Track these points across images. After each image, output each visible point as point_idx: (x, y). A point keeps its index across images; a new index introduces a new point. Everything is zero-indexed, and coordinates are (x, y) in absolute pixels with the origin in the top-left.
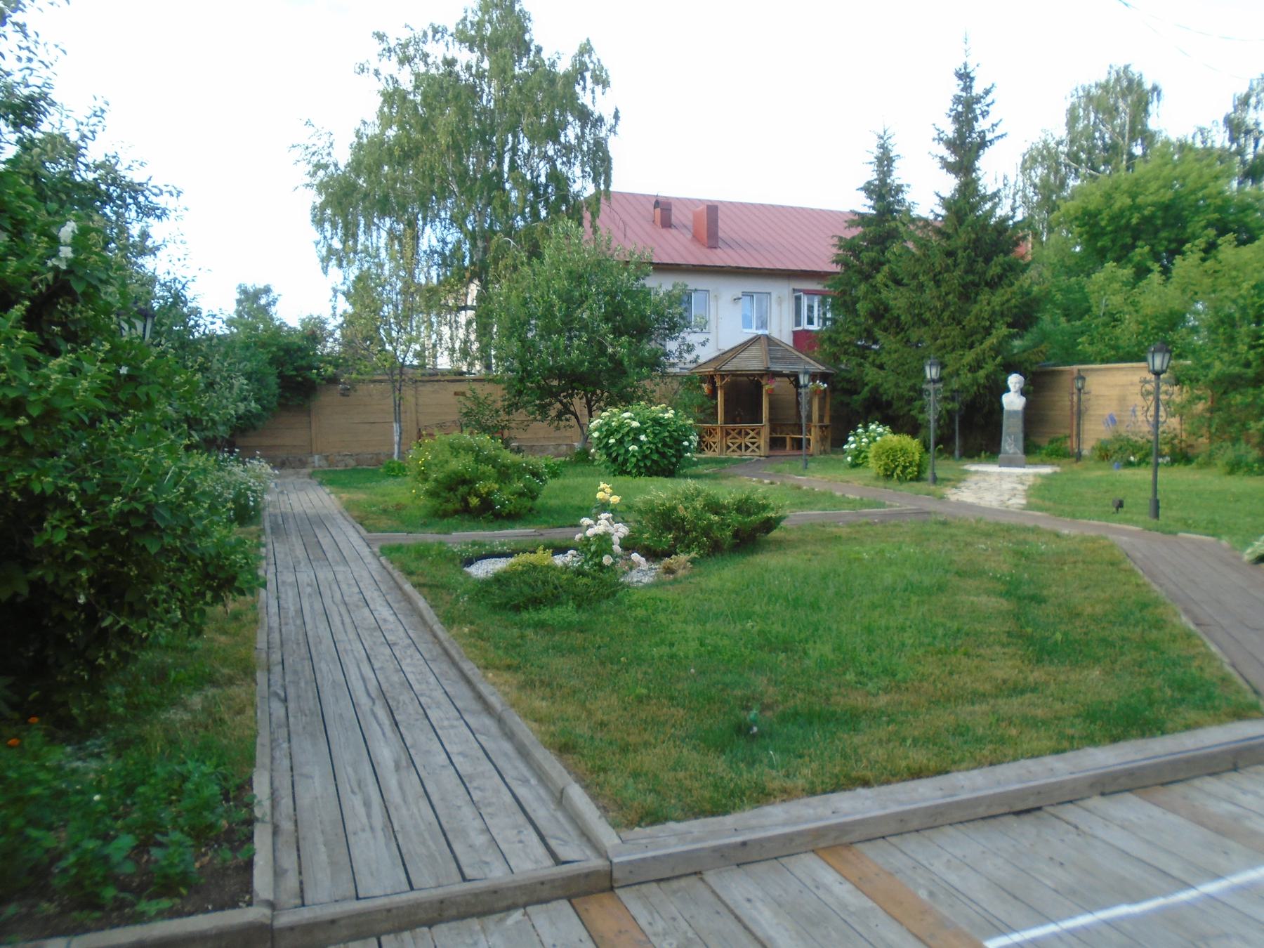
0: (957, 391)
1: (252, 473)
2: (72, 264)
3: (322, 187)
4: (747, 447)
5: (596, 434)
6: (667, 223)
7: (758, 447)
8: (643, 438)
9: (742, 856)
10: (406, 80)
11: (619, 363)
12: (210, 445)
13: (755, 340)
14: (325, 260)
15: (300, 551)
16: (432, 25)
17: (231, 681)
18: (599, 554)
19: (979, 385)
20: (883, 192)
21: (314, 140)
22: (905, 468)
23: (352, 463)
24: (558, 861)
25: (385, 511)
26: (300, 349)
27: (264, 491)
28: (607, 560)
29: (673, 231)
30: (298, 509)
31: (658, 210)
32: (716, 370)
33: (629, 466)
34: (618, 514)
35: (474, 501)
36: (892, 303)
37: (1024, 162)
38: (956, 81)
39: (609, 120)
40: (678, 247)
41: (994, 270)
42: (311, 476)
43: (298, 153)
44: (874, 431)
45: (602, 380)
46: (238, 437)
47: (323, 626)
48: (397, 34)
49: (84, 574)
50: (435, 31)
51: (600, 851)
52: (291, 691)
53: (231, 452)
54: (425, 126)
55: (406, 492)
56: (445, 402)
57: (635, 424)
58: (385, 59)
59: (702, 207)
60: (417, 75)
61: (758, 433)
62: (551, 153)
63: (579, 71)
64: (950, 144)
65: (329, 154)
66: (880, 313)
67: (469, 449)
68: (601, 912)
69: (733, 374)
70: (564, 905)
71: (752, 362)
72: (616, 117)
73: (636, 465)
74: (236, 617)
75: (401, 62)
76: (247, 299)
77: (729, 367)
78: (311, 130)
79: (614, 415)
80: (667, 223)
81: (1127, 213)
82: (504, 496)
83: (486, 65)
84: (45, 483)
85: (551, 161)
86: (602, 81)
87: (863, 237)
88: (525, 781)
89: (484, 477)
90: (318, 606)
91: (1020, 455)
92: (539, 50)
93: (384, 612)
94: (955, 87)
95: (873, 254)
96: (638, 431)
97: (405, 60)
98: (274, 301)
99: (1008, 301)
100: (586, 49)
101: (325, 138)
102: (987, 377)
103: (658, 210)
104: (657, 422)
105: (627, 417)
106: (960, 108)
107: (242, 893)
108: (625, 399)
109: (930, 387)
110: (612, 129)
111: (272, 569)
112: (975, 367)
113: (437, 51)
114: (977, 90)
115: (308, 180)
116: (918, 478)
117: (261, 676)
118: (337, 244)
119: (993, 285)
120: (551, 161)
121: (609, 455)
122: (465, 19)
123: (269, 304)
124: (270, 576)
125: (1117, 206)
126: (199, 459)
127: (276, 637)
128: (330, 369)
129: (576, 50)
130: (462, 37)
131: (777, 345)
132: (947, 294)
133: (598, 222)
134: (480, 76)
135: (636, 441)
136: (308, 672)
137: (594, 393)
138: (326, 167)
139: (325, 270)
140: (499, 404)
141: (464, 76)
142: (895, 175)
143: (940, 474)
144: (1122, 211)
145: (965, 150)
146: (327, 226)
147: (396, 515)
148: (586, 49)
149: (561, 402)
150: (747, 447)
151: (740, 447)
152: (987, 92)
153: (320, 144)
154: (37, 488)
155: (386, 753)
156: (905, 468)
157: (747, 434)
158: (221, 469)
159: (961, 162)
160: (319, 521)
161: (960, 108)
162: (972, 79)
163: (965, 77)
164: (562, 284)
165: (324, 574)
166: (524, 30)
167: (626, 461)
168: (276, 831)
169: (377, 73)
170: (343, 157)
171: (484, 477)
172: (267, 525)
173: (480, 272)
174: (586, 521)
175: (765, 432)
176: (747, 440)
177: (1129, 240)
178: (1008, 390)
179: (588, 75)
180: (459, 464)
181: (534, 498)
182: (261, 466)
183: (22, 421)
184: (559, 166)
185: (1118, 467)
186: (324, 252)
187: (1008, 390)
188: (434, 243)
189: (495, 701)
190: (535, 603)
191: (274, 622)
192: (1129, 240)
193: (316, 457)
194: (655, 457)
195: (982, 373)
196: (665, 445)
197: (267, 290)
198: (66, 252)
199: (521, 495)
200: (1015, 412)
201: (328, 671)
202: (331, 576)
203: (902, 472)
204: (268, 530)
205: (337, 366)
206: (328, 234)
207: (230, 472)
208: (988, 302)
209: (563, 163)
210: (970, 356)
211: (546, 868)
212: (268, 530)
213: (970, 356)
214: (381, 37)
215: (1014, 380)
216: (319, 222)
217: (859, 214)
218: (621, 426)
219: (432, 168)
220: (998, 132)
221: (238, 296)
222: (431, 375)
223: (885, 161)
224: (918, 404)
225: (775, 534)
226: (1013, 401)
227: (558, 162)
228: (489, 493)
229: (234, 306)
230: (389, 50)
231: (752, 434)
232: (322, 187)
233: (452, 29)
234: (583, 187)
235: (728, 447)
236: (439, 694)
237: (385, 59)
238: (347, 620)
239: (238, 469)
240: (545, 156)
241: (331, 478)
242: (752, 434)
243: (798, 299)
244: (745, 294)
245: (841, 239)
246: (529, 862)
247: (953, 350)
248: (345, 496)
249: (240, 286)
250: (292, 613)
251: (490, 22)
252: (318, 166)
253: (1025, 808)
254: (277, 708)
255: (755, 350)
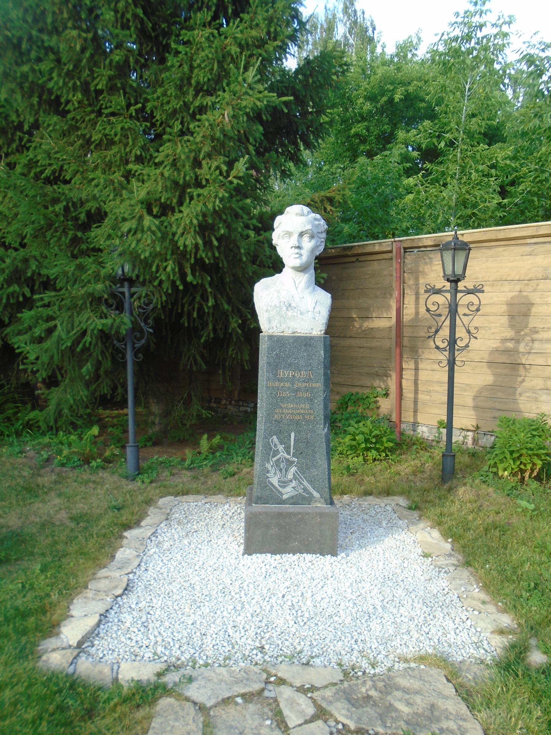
0: (126, 280)
19: (181, 255)
102: (204, 229)
187: (277, 266)
195: (189, 214)
200: (304, 342)
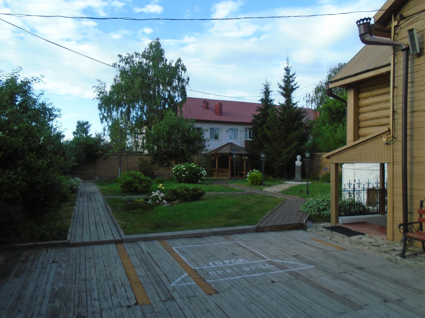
1: (76, 181)
2: (42, 143)
3: (101, 99)
4: (224, 176)
5: (174, 172)
6: (207, 108)
7: (228, 176)
8: (186, 173)
9: (145, 240)
10: (127, 67)
11: (183, 151)
12: (65, 173)
13: (228, 144)
14: (102, 120)
15: (86, 199)
16: (135, 53)
17: (66, 219)
18: (156, 200)
20: (266, 101)
21: (100, 85)
22: (257, 182)
23: (107, 179)
24: (114, 238)
25: (111, 191)
26: (93, 145)
27: (78, 185)
28: (158, 202)
29: (209, 110)
30: (88, 190)
31: (205, 104)
32: (216, 153)
33: (183, 181)
34: (162, 191)
35: (133, 189)
36: (267, 134)
37: (315, 91)
38: (285, 71)
39: (186, 80)
40: (211, 115)
41: (295, 125)
42: (94, 182)
43: (94, 89)
44: (255, 171)
45: (180, 157)
46: (73, 171)
47: (87, 213)
48: (124, 55)
49: (42, 195)
50: (136, 54)
51: (121, 237)
52: (78, 221)
53: (71, 175)
54: (132, 82)
55: (117, 187)
56: (135, 161)
57: (184, 169)
58: (121, 62)
59: (217, 104)
60: (131, 67)
61: (228, 172)
62: (169, 89)
63: (177, 67)
64: (283, 89)
65: (104, 89)
66: (264, 136)
67: (132, 175)
68: (119, 245)
69: (220, 154)
70: (114, 244)
71: (226, 151)
72: (188, 79)
73: (184, 180)
74: (68, 210)
75: (126, 63)
76: (80, 126)
77: (219, 152)
78: (100, 82)
79: (179, 166)
80: (207, 108)
81: (340, 108)
82: (140, 187)
83: (151, 64)
84: (38, 180)
85: (169, 92)
86: (184, 69)
87: (261, 114)
88: (115, 232)
89: (135, 182)
90: (87, 209)
91: (300, 179)
92: (166, 60)
93: (101, 211)
94: (284, 73)
95: (263, 120)
96: (185, 171)
97: (127, 63)
98: (89, 127)
99: (298, 134)
100: (179, 60)
101: (103, 84)
103: (205, 104)
104: (191, 168)
105: (183, 167)
106: (286, 79)
107: (66, 239)
108: (184, 161)
109: (263, 160)
110: (187, 83)
111: (78, 203)
112: (288, 153)
113: (137, 60)
114: (291, 74)
115: (98, 97)
116: (261, 184)
117: (72, 219)
118: (106, 115)
119: (295, 129)
120: (169, 92)
121: (177, 177)
122: (145, 51)
123: (87, 128)
124: (77, 204)
125: (337, 105)
126: (62, 177)
127: (76, 214)
128: (101, 152)
129: (176, 61)
130: (144, 56)
131: (234, 145)
132: (282, 132)
133: (182, 109)
134: (149, 67)
135: (184, 173)
136: (82, 219)
137: (177, 160)
138: (103, 93)
139: (102, 122)
140: (149, 162)
141: (145, 67)
142: (270, 96)
143: (265, 183)
144: (338, 107)
145: (288, 90)
146: (103, 109)
147: (114, 192)
148: (179, 60)
149: (168, 162)
150: (224, 176)
151: (222, 175)
152: (293, 75)
153: (102, 86)
154: (36, 181)
155: (92, 229)
156: (257, 182)
157: (224, 172)
158: (68, 180)
159: (286, 94)
160: (93, 193)
161: (286, 79)
162: (290, 71)
163: (287, 70)
164: (167, 129)
165: (90, 204)
166: (162, 54)
167: (182, 179)
168: (71, 236)
169: (119, 66)
170: (108, 89)
171: (135, 182)
172: (79, 194)
173: (147, 123)
174: (153, 192)
175: (229, 171)
176: (224, 174)
177: (341, 116)
178: (297, 160)
179: (180, 67)
180: (129, 179)
181: (148, 188)
182: (78, 179)
183: (35, 170)
184: (171, 93)
185: (326, 182)
186: (102, 117)
187: (297, 160)
188: (134, 114)
189: (116, 223)
190: (133, 209)
191: (77, 211)
192: (341, 116)
193: (97, 177)
194: (190, 178)
195: (290, 155)
196: (193, 174)
197: (87, 123)
198: (41, 142)
199: (145, 187)
200: (299, 166)
201: (86, 219)
202: (91, 204)
203: (256, 183)
204: (79, 195)
205: (103, 151)
206: (103, 112)
207: (70, 181)
208: (294, 134)
209: (173, 92)
210: (288, 150)
211: (112, 238)
212: (79, 195)
213: (288, 150)
214: (120, 56)
215: (299, 157)
216: (100, 108)
217: (260, 108)
218: (181, 169)
219: (134, 94)
220: (296, 86)
221: (77, 125)
222: (135, 153)
223: (267, 92)
224: (274, 163)
225: (203, 197)
226: (298, 163)
227: (171, 92)
228: (137, 186)
229: (76, 128)
230: (123, 60)
231: (226, 172)
232: (101, 99)
233: (141, 54)
234: (178, 99)
235: (219, 176)
236: (106, 222)
237: (121, 62)
238: (93, 212)
239: (72, 180)
240: (167, 90)
241: (98, 183)
242: (226, 172)
243: (246, 131)
244: (230, 129)
245: (254, 114)
246: (110, 238)
247: (284, 148)
248: (101, 188)
249: (78, 122)
250: (81, 210)
251: (152, 52)
252: (101, 93)
253: (198, 236)
254: (75, 223)
255: (227, 147)
